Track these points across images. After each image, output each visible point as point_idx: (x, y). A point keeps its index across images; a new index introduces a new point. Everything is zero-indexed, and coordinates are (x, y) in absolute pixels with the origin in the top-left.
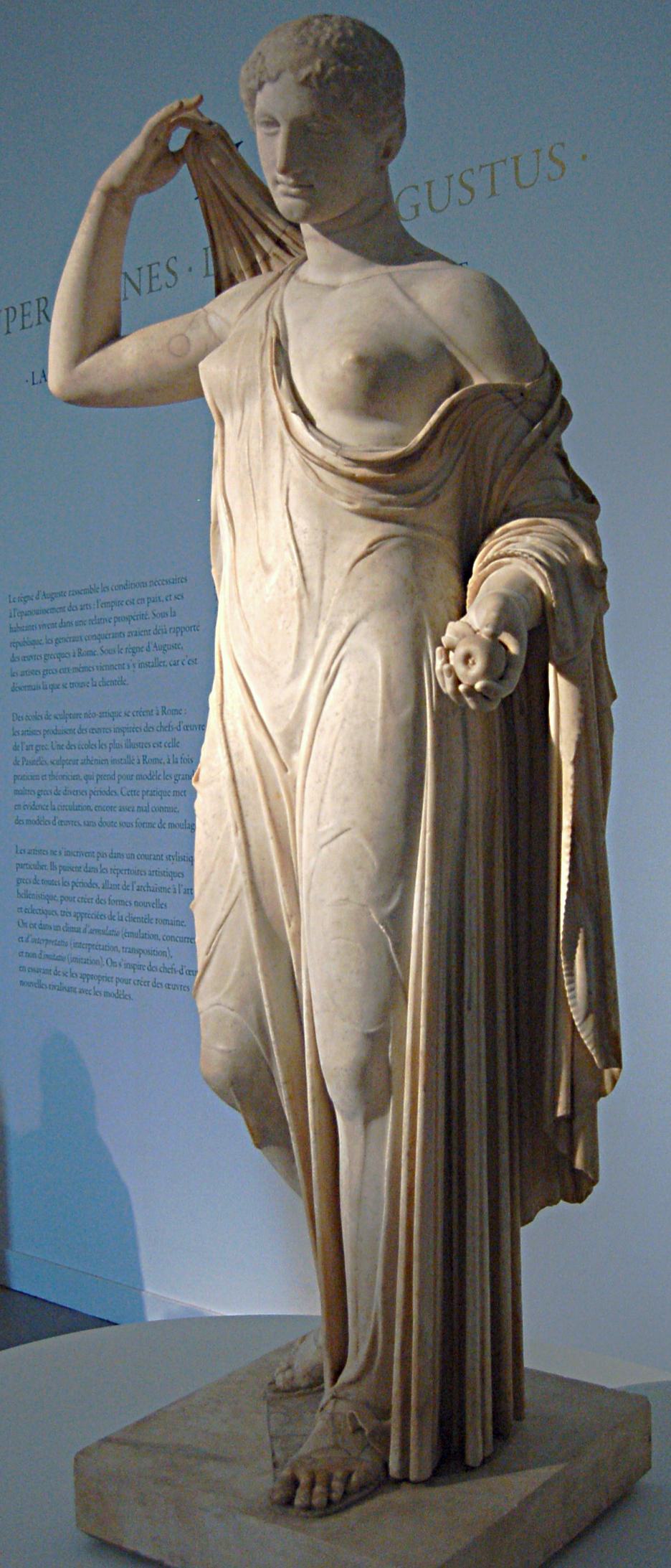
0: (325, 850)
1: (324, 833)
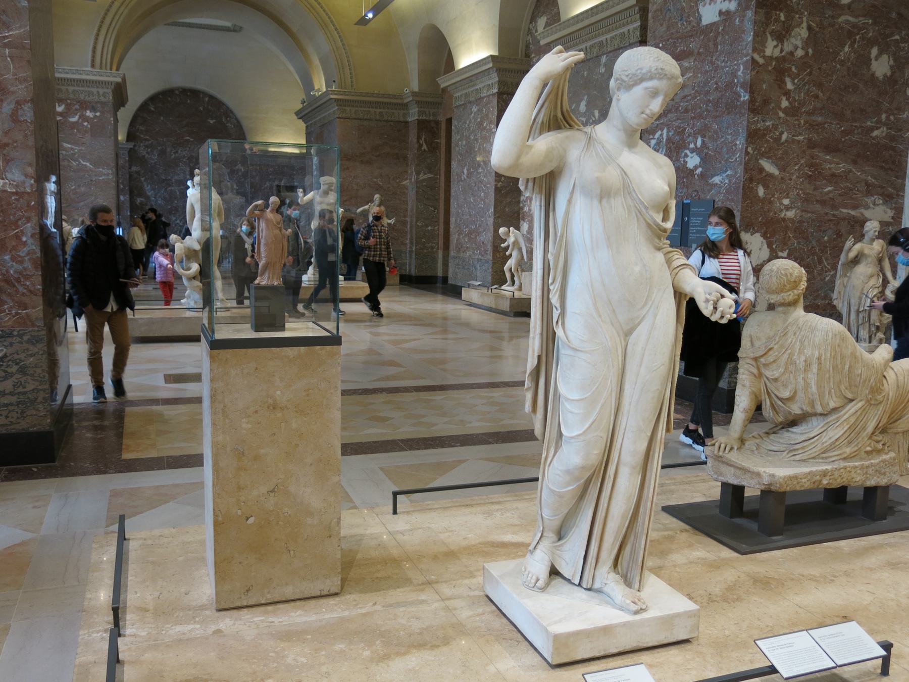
0: (654, 372)
1: (655, 366)
